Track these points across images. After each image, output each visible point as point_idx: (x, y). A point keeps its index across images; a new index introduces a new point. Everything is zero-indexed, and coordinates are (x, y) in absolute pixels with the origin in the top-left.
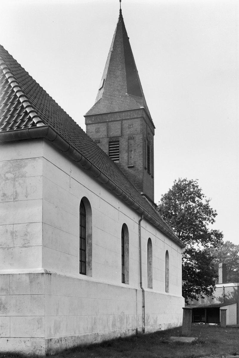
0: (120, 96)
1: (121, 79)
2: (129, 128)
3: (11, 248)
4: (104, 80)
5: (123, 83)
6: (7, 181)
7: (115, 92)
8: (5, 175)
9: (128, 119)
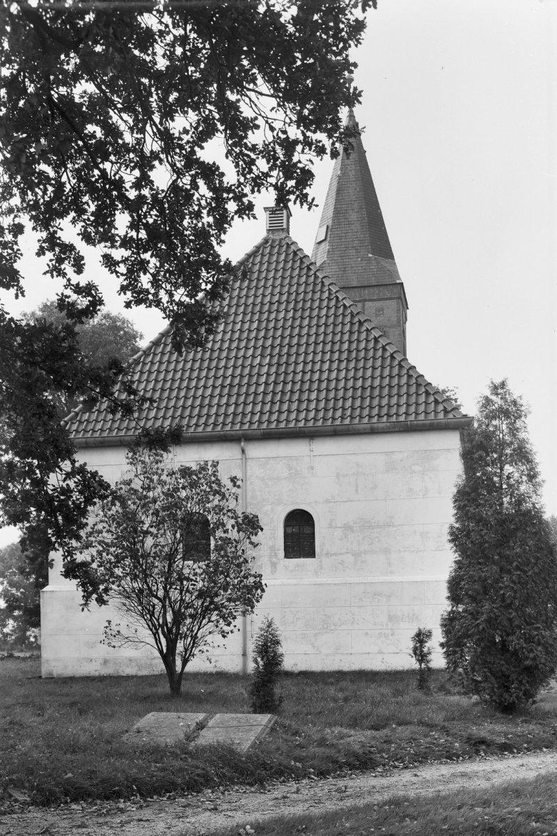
0: (359, 259)
1: (360, 228)
2: (377, 316)
3: (421, 551)
4: (328, 227)
5: (362, 236)
6: (413, 475)
7: (350, 251)
8: (411, 467)
9: (375, 300)
